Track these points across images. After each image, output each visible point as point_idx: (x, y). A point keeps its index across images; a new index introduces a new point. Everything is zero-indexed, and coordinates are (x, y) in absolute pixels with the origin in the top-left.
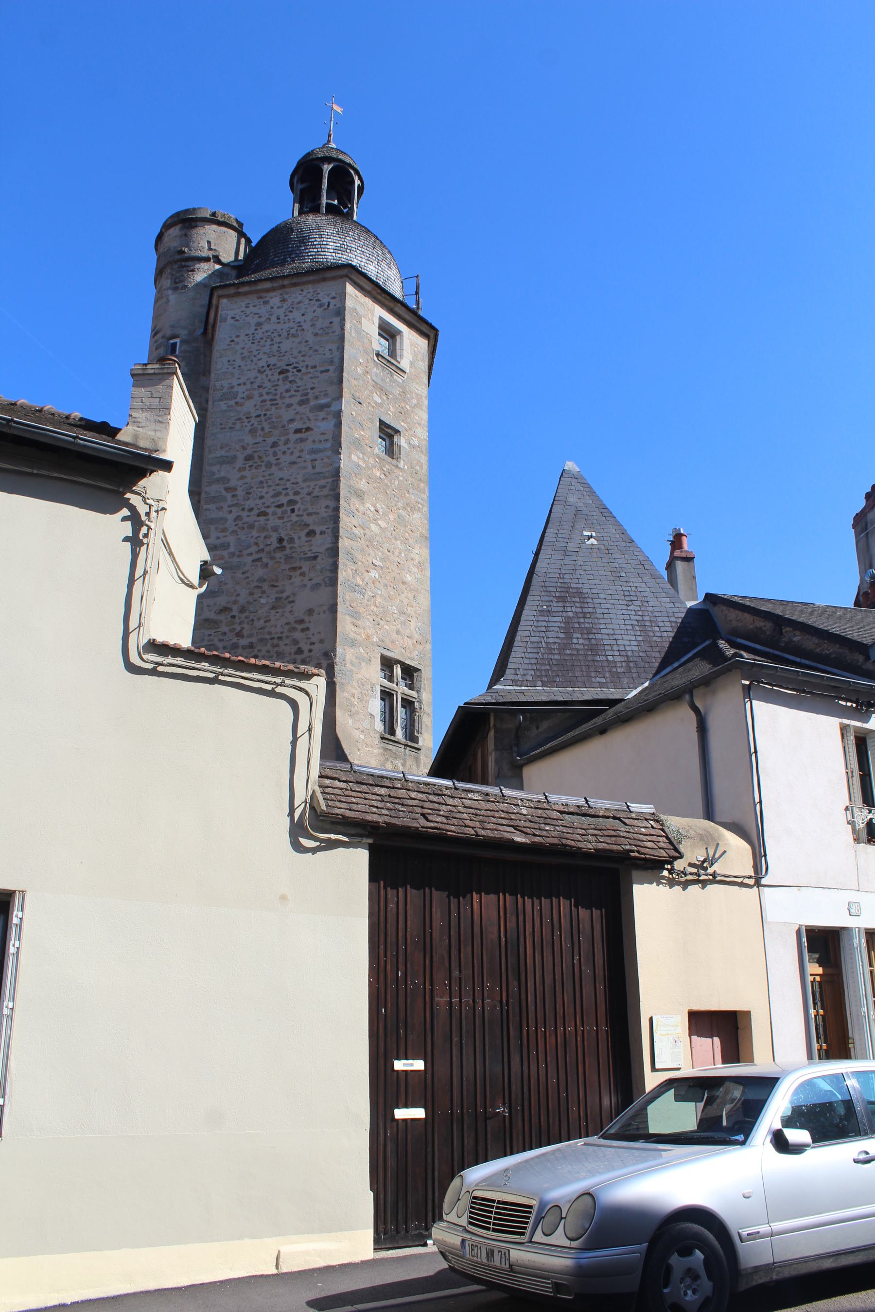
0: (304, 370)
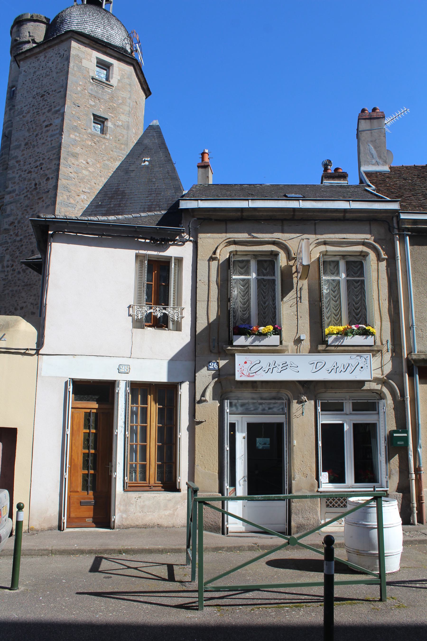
0: (51, 93)
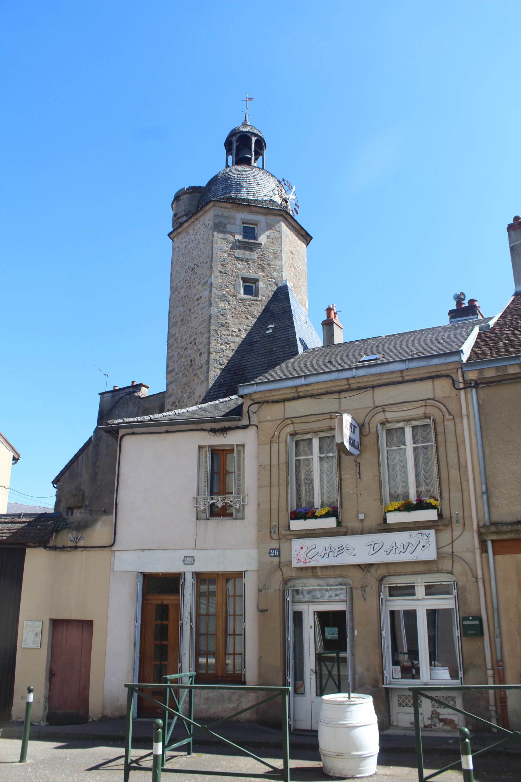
0: (199, 265)
